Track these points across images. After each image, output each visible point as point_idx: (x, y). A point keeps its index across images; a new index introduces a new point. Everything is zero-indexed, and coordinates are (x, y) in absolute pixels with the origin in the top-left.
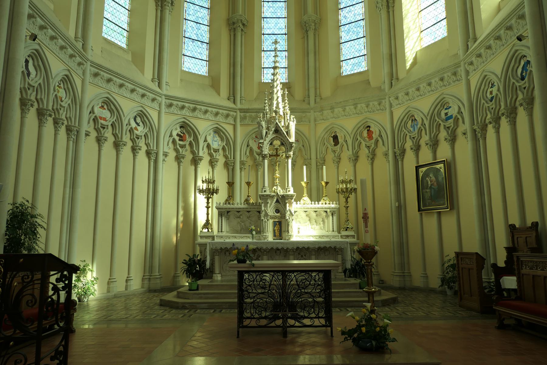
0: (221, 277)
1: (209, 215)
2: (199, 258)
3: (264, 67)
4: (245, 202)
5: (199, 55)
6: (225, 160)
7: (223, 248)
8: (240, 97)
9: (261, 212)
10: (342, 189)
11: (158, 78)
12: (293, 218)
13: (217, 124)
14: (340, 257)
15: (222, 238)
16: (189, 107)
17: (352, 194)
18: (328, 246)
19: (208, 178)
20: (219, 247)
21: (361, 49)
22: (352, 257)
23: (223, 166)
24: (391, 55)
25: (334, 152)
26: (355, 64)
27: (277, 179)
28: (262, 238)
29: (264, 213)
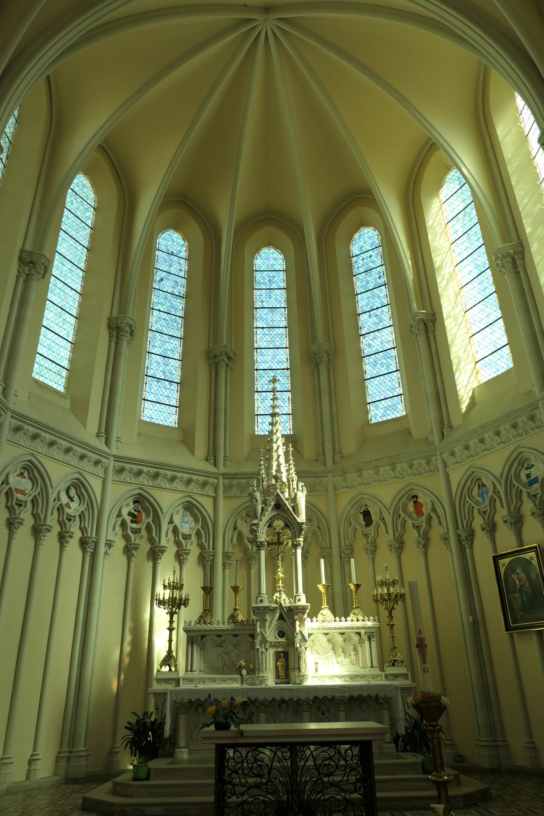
1: (173, 642)
2: (152, 719)
4: (230, 620)
5: (165, 399)
8: (224, 457)
9: (256, 636)
10: (382, 596)
12: (307, 644)
13: (189, 496)
15: (191, 681)
17: (397, 604)
18: (365, 694)
19: (172, 581)
20: (186, 700)
21: (395, 387)
22: (406, 713)
25: (366, 535)
27: (280, 581)
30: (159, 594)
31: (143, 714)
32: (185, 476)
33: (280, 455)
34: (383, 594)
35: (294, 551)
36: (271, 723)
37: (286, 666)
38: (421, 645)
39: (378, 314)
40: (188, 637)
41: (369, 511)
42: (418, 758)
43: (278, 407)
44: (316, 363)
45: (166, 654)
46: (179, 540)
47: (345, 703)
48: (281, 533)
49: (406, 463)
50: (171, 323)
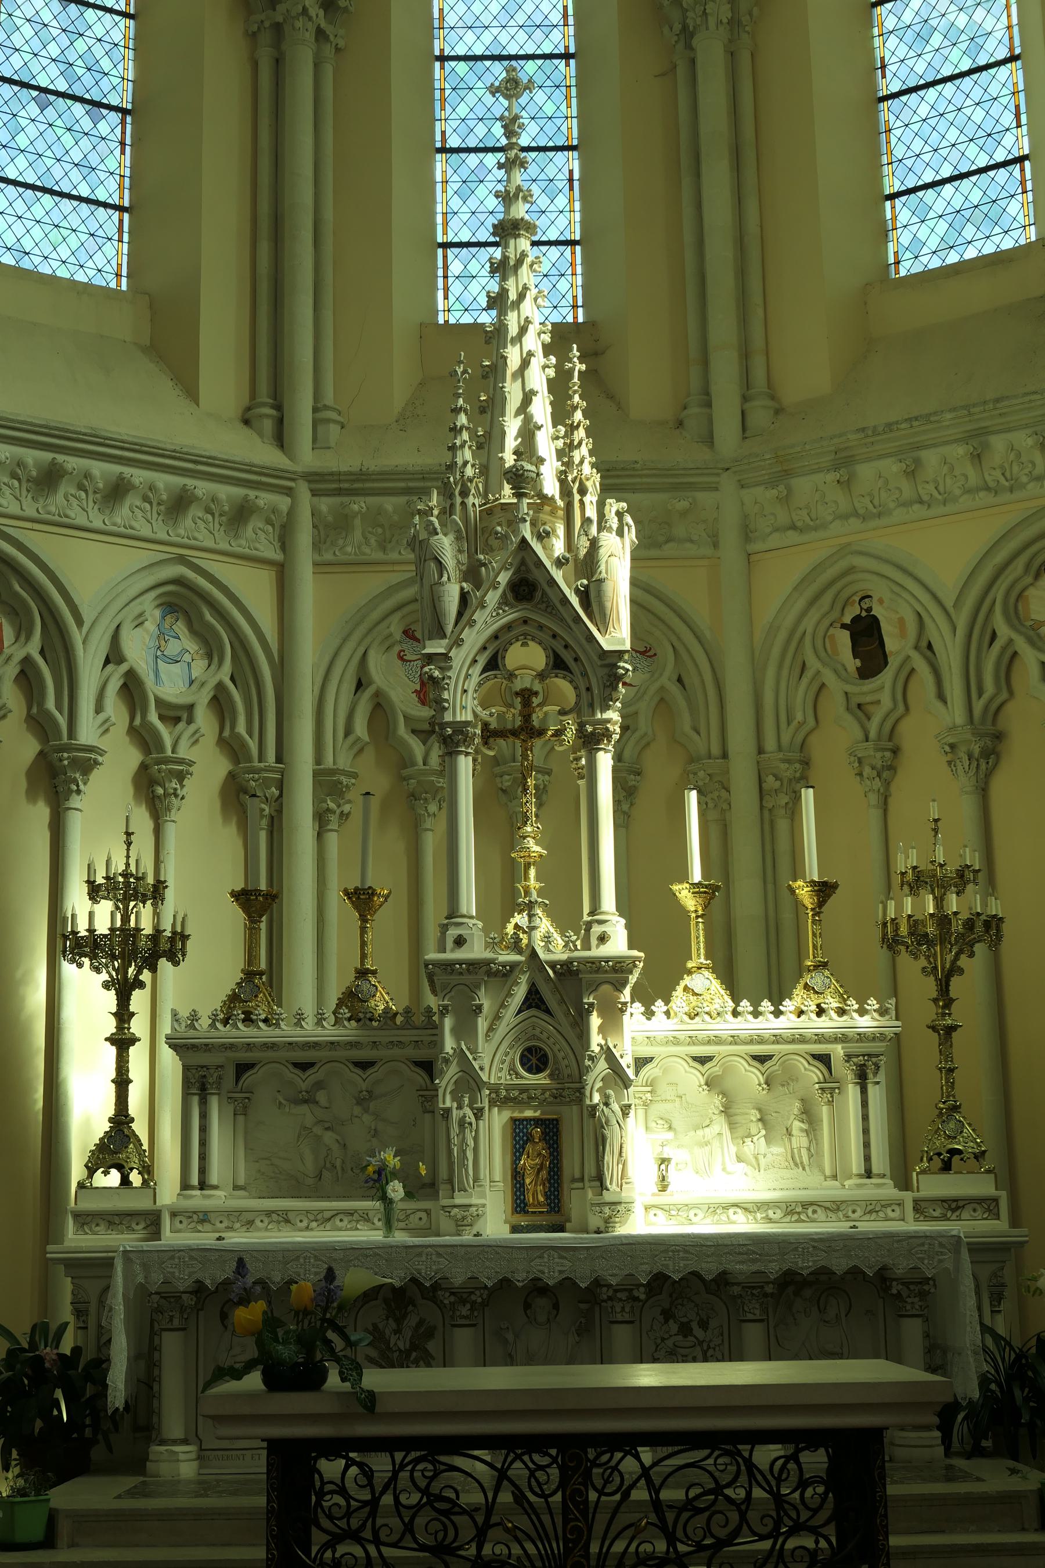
0: (195, 1464)
1: (131, 1087)
2: (66, 1347)
3: (451, 237)
4: (344, 1010)
5: (75, 175)
6: (231, 768)
7: (208, 1282)
8: (315, 410)
9: (439, 1064)
10: (914, 924)
12: (633, 1095)
13: (182, 560)
14: (912, 1330)
15: (202, 1221)
16: (20, 464)
17: (972, 955)
18: (840, 1265)
19: (121, 868)
20: (183, 1282)
21: (999, 128)
22: (985, 1329)
23: (217, 804)
25: (861, 710)
26: (967, 214)
27: (532, 872)
28: (445, 1223)
29: (452, 1072)
30: (73, 916)
31: (29, 1331)
32: (164, 481)
33: (533, 393)
34: (921, 918)
35: (583, 761)
36: (494, 1364)
37: (551, 1169)
40: (186, 1069)
41: (875, 620)
42: (1025, 1478)
43: (525, 199)
44: (685, 27)
45: (106, 1126)
46: (147, 725)
47: (766, 1295)
48: (536, 694)
49: (1029, 431)
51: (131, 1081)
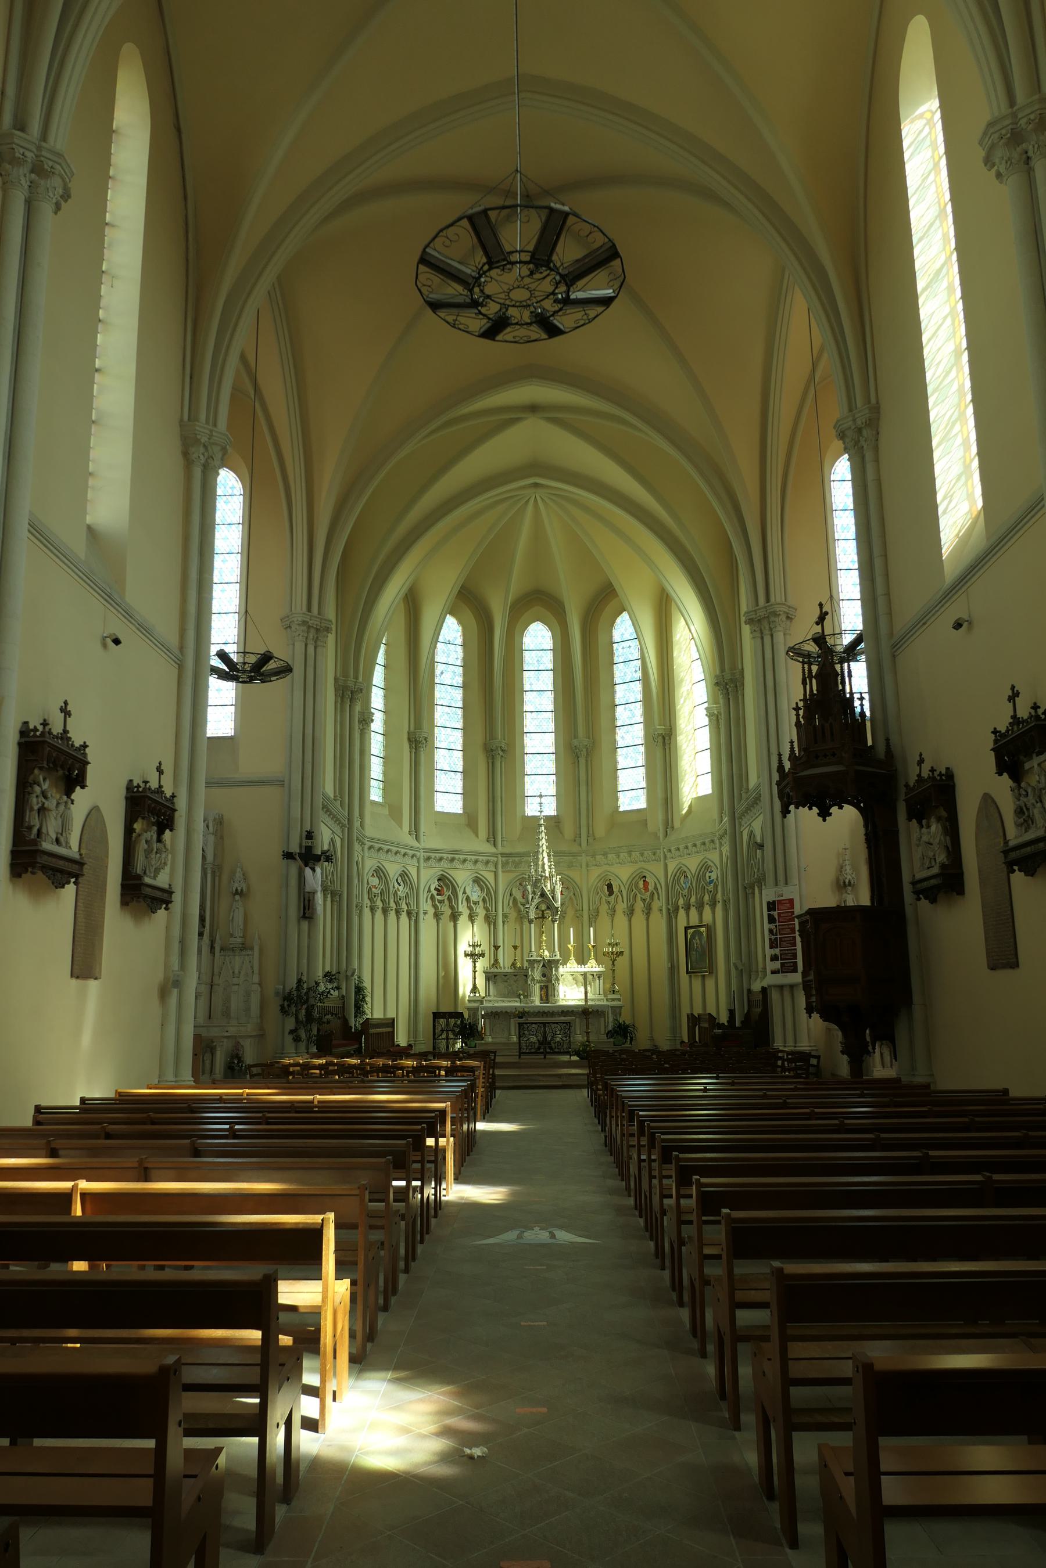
11: (415, 830)
13: (477, 873)
24: (666, 800)
29: (531, 977)
32: (473, 858)
38: (192, 1111)
39: (632, 708)
50: (452, 716)
51: (89, 763)
